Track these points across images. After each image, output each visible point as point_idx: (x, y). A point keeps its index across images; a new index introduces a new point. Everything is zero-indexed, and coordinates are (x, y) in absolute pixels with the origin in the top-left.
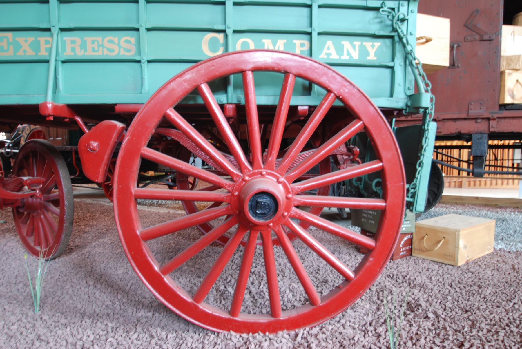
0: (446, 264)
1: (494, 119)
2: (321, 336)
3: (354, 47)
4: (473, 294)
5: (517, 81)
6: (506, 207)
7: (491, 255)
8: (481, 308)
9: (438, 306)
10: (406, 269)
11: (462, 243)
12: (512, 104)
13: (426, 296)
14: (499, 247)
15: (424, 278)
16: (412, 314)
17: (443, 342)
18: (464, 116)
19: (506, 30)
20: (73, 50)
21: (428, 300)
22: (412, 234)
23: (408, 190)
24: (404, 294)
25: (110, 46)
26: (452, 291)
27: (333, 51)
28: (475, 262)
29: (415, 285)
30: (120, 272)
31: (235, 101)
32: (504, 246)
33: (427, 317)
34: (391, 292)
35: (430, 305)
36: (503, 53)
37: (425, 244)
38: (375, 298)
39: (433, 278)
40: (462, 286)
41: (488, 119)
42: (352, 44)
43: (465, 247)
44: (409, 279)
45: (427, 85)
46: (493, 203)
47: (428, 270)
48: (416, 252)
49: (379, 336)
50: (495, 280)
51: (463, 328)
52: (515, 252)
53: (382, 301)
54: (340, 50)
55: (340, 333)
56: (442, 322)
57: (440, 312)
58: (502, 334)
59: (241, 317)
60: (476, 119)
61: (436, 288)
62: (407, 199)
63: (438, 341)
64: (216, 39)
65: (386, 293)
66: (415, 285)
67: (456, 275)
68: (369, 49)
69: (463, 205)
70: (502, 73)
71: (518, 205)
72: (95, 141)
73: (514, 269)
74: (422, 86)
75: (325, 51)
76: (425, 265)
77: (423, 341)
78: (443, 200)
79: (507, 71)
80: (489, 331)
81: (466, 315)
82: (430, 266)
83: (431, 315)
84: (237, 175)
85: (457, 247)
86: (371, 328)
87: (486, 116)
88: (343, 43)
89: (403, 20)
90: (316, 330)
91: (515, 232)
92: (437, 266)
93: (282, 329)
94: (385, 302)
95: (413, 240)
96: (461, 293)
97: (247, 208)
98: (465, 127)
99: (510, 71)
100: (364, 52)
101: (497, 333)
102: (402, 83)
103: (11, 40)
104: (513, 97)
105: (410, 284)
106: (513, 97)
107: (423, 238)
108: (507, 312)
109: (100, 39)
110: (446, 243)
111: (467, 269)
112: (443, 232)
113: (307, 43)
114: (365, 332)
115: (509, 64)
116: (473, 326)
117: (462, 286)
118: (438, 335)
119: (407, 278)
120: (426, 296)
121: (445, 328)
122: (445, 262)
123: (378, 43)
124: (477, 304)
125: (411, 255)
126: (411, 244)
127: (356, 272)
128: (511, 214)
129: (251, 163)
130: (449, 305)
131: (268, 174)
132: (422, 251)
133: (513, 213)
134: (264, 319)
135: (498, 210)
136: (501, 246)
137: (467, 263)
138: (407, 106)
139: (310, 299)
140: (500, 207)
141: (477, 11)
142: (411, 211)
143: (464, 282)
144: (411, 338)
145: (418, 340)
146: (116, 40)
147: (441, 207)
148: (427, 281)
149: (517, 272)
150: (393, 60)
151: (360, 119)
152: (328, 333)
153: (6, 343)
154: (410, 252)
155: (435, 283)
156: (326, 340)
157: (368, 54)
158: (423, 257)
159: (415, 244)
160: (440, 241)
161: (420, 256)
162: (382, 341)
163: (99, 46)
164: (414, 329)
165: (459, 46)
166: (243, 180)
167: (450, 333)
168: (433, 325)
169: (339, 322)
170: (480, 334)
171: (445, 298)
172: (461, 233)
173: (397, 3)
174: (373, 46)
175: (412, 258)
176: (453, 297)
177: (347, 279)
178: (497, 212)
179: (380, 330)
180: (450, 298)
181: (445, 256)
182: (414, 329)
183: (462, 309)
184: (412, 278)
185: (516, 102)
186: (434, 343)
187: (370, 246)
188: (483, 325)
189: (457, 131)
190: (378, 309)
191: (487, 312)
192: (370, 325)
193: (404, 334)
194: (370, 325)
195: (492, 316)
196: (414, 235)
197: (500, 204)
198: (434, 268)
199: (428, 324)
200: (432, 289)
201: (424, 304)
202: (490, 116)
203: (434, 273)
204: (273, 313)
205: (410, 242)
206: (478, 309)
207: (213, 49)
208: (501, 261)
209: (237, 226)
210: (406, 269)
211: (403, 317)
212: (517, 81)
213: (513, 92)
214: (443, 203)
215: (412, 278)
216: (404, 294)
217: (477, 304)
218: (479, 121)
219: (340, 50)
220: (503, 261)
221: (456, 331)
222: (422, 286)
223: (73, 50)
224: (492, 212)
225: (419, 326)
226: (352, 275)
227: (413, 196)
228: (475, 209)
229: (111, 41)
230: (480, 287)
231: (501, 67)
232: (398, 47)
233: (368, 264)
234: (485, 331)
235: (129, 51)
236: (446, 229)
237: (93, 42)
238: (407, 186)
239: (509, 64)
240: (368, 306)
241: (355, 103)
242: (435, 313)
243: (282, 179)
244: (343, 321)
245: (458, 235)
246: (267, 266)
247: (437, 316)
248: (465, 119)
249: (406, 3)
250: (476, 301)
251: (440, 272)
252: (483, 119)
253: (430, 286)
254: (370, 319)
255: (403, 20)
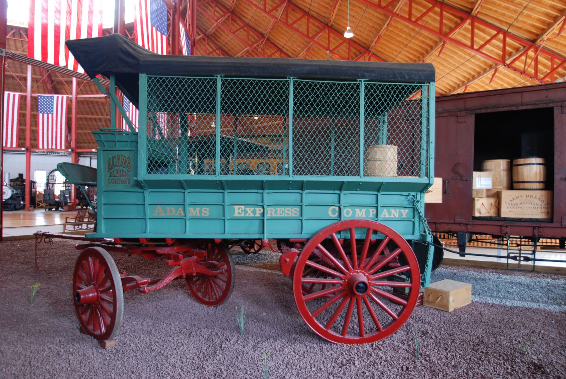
0: (442, 311)
1: (470, 225)
2: (384, 345)
3: (396, 212)
4: (455, 327)
5: (482, 204)
6: (488, 268)
7: (469, 306)
8: (458, 334)
9: (437, 333)
10: (420, 313)
11: (451, 299)
12: (480, 217)
13: (431, 328)
14: (476, 300)
15: (430, 318)
16: (424, 336)
17: (439, 348)
18: (453, 222)
19: (476, 174)
20: (271, 214)
21: (432, 330)
22: (423, 293)
23: (421, 277)
24: (420, 327)
25: (288, 212)
26: (445, 326)
27: (387, 214)
28: (459, 310)
29: (425, 322)
30: (264, 314)
31: (344, 238)
32: (478, 300)
33: (432, 338)
34: (413, 326)
35: (433, 332)
36: (474, 188)
37: (431, 299)
38: (405, 329)
39: (435, 319)
40: (450, 323)
41: (467, 225)
42: (395, 210)
43: (453, 301)
44: (422, 319)
45: (429, 231)
46: (479, 265)
47: (432, 314)
48: (425, 303)
49: (410, 345)
50: (469, 320)
51: (448, 342)
52: (484, 303)
53: (409, 330)
54: (390, 213)
55: (393, 344)
56: (438, 340)
57: (438, 336)
58: (465, 345)
59: (347, 337)
60: (459, 224)
61: (436, 324)
62: (421, 281)
63: (436, 348)
64: (335, 209)
65: (411, 326)
66: (425, 322)
67: (448, 317)
68: (403, 212)
69: (458, 266)
70: (473, 199)
71: (497, 267)
72: (288, 258)
73: (480, 314)
74: (427, 231)
75: (383, 214)
76: (431, 311)
77: (429, 347)
78: (443, 262)
79: (476, 199)
80: (460, 344)
81: (450, 337)
82: (434, 312)
83: (433, 337)
84: (347, 273)
85: (448, 301)
86: (406, 342)
87: (465, 223)
88: (391, 210)
89: (418, 201)
90: (381, 343)
91: (488, 289)
92: (437, 312)
93: (365, 342)
94: (411, 331)
95: (424, 296)
96: (449, 327)
97: (355, 290)
98: (454, 228)
99: (478, 198)
100: (401, 214)
101: (463, 345)
102: (418, 228)
103: (243, 209)
104: (480, 213)
105: (423, 322)
106: (480, 213)
107: (430, 295)
108: (470, 336)
109: (283, 209)
110: (442, 298)
111: (454, 314)
112: (441, 293)
113: (375, 210)
114: (404, 344)
115: (477, 194)
116: (453, 342)
117: (450, 323)
118: (437, 345)
119: (421, 319)
120: (431, 328)
121: (440, 343)
122: (442, 309)
123: (407, 210)
124: (456, 332)
125: (423, 305)
126: (423, 298)
127: (398, 315)
128: (490, 274)
129: (353, 267)
130: (442, 332)
131: (361, 272)
132: (429, 302)
133: (491, 274)
134: (357, 338)
135: (482, 270)
136: (477, 299)
137: (455, 310)
138: (420, 239)
139: (378, 329)
140: (484, 268)
141: (459, 163)
142: (423, 287)
143: (451, 321)
144: (424, 346)
145: (427, 347)
146: (290, 209)
147: (443, 267)
148: (432, 320)
149: (482, 316)
150: (414, 218)
151: (400, 248)
152: (387, 344)
153: (479, 316)
154: (422, 303)
155: (436, 321)
156: (386, 347)
157: (403, 215)
158: (430, 306)
159: (425, 299)
160: (439, 297)
161: (428, 306)
162: (411, 347)
163: (283, 212)
164: (426, 343)
165: (448, 182)
166: (350, 275)
167: (442, 344)
168: (434, 341)
169: (391, 339)
170: (456, 345)
171: (441, 329)
172: (450, 293)
173: (415, 193)
174: (405, 211)
175: (424, 307)
176: (444, 329)
177: (394, 319)
178: (481, 272)
179: (410, 343)
180: (443, 329)
181: (442, 306)
182: (426, 343)
183: (448, 334)
184: (424, 319)
185: (482, 216)
186: (434, 348)
187: (405, 304)
188: (457, 341)
189: (448, 230)
190: (408, 334)
191: (461, 336)
192: (405, 341)
193: (421, 345)
194: (405, 341)
195: (462, 338)
196: (424, 293)
197: (484, 266)
198: (435, 313)
199: (432, 341)
200: (434, 325)
201: (430, 332)
202: (467, 223)
203: (436, 316)
204: (361, 334)
205: (422, 297)
206: (457, 334)
207: (334, 214)
208: (474, 309)
209: (57, 193)
210: (420, 313)
211: (420, 338)
212: (482, 204)
213: (480, 210)
214: (445, 264)
215: (424, 319)
216: (420, 327)
217: (456, 332)
218: (461, 225)
219: (390, 213)
220: (476, 309)
221: (445, 344)
222: (429, 323)
223: (271, 214)
224: (478, 272)
225: (428, 342)
226: (396, 317)
227: (424, 280)
228: (466, 269)
229: (288, 210)
230: (459, 324)
231: (473, 195)
232: (416, 212)
233: (404, 312)
234: (458, 344)
235: (296, 214)
236: (442, 290)
237: (280, 210)
238: (421, 275)
239: (477, 194)
240: (402, 333)
241: (397, 241)
242: (435, 336)
243: (366, 274)
244: (392, 339)
245: (449, 294)
246: (359, 313)
247: (436, 337)
248: (453, 223)
249: (419, 193)
250: (457, 330)
251: (439, 315)
252: (463, 224)
253: (433, 323)
254: (404, 338)
255: (418, 201)
